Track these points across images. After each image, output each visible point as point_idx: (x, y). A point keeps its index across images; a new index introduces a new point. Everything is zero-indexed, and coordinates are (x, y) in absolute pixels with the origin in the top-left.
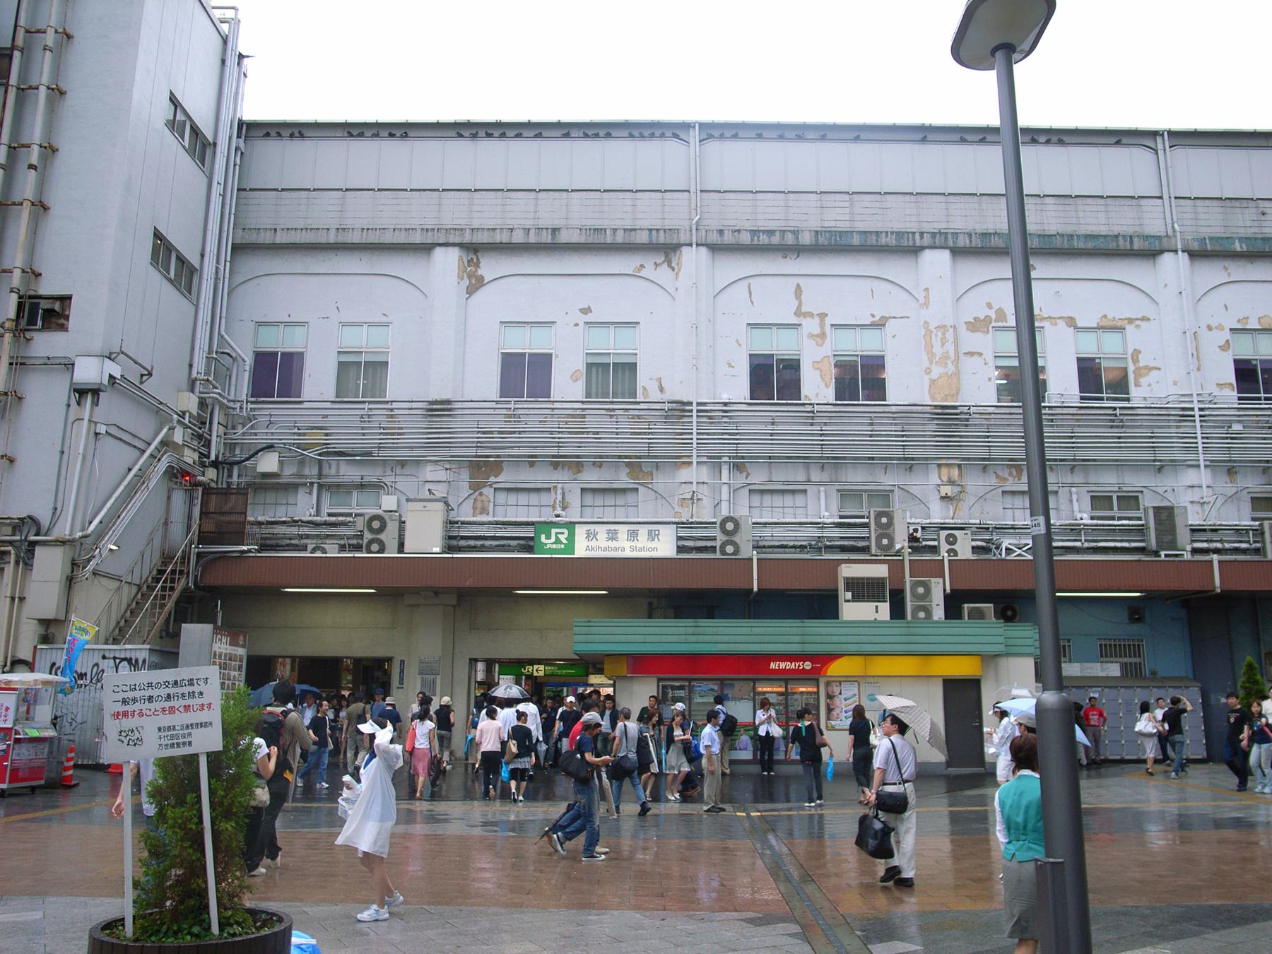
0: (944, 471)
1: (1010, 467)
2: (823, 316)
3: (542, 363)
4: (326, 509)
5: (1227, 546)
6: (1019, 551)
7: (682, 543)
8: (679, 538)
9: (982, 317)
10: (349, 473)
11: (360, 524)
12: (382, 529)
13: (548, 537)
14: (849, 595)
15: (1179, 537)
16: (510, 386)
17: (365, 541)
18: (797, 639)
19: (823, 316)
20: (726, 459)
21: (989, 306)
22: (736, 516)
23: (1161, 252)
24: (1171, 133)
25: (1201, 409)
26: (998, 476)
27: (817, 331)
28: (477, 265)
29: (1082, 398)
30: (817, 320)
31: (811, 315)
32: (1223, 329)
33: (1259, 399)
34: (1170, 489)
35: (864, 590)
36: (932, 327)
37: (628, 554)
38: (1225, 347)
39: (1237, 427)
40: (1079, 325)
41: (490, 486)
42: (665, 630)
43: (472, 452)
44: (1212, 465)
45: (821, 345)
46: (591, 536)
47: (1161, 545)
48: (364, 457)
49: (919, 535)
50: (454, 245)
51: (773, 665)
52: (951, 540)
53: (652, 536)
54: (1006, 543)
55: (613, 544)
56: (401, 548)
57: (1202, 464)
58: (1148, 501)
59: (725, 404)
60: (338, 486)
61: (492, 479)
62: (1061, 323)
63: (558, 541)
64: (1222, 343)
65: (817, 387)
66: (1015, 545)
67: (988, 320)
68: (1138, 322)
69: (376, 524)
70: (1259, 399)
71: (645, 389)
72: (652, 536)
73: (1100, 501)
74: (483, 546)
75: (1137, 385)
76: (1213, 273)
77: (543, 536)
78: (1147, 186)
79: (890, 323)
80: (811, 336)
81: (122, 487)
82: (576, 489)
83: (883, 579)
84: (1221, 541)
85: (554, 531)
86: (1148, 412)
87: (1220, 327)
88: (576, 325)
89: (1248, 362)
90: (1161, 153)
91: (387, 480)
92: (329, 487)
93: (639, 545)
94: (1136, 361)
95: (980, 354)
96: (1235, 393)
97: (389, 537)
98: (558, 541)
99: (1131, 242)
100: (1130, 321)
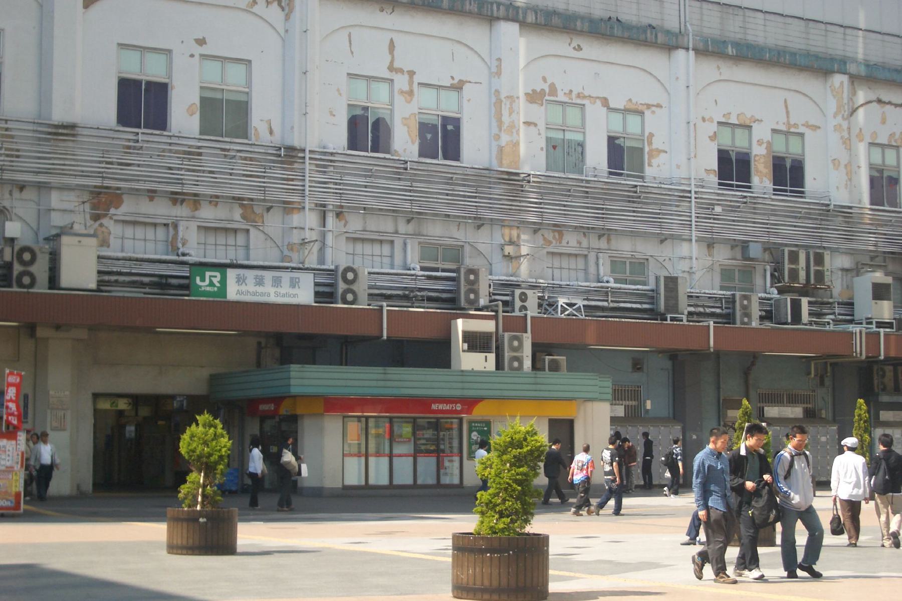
0: (507, 231)
1: (554, 231)
2: (412, 74)
5: (708, 310)
6: (570, 310)
7: (321, 289)
9: (538, 90)
13: (203, 280)
14: (466, 346)
15: (680, 302)
17: (340, 291)
18: (460, 385)
19: (412, 74)
20: (331, 207)
21: (544, 79)
22: (355, 267)
23: (677, 47)
25: (696, 192)
26: (545, 239)
27: (406, 88)
29: (610, 173)
30: (406, 77)
31: (400, 71)
32: (712, 122)
33: (786, 191)
34: (667, 259)
35: (476, 342)
36: (502, 97)
37: (273, 299)
38: (714, 137)
39: (718, 209)
40: (612, 106)
41: (111, 218)
42: (362, 376)
43: (97, 182)
44: (699, 240)
45: (409, 102)
46: (240, 280)
51: (434, 407)
53: (294, 283)
54: (562, 301)
55: (260, 289)
57: (694, 239)
58: (653, 271)
59: (332, 154)
62: (599, 102)
64: (711, 134)
65: (405, 143)
66: (567, 304)
68: (654, 109)
70: (786, 191)
71: (256, 130)
72: (294, 283)
73: (616, 265)
74: (116, 281)
76: (710, 69)
77: (198, 279)
79: (466, 87)
80: (402, 92)
82: (193, 225)
83: (491, 333)
84: (703, 306)
85: (208, 274)
86: (94, 132)
87: (711, 120)
88: (192, 56)
89: (727, 152)
93: (283, 291)
94: (650, 143)
95: (535, 125)
96: (771, 186)
98: (211, 284)
100: (649, 106)
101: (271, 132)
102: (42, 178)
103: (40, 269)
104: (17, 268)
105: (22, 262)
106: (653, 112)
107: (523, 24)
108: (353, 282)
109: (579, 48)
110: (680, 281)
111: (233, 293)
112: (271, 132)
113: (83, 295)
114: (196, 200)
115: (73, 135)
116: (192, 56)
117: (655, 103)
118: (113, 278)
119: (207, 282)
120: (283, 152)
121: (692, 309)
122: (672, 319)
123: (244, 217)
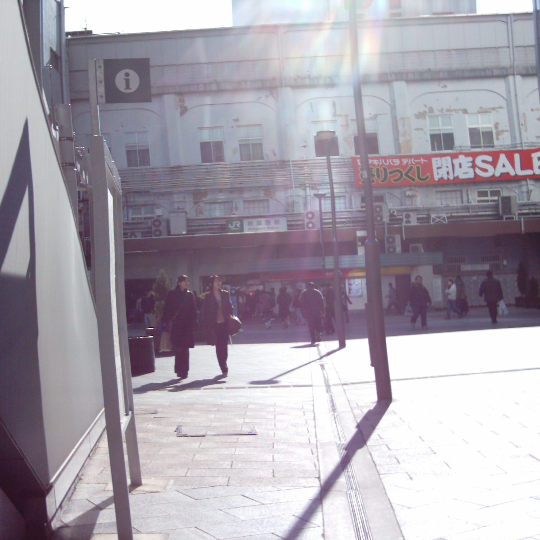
3: (219, 146)
4: (131, 216)
6: (438, 219)
7: (289, 223)
8: (288, 221)
9: (417, 113)
10: (140, 200)
11: (150, 222)
12: (160, 224)
13: (232, 225)
16: (206, 158)
20: (308, 185)
21: (425, 106)
24: (515, 15)
28: (183, 101)
43: (194, 188)
47: (504, 213)
48: (146, 193)
49: (395, 214)
50: (172, 93)
52: (408, 216)
54: (433, 216)
56: (169, 233)
60: (135, 206)
61: (203, 199)
62: (460, 112)
63: (236, 227)
67: (425, 113)
68: (498, 110)
69: (157, 223)
72: (276, 222)
75: (497, 139)
78: (502, 41)
81: (76, 447)
85: (234, 223)
90: (509, 24)
91: (157, 202)
92: (131, 206)
95: (422, 129)
97: (163, 228)
98: (236, 227)
99: (492, 72)
101: (275, 155)
102: (168, 190)
103: (163, 228)
104: (154, 228)
105: (155, 226)
106: (498, 112)
107: (408, 81)
108: (312, 218)
109: (445, 86)
110: (512, 199)
111: (247, 231)
112: (275, 155)
113: (147, 239)
114: (241, 190)
115: (181, 170)
116: (232, 127)
117: (498, 106)
118: (201, 228)
119: (234, 226)
120: (346, 161)
121: (520, 212)
122: (507, 218)
123: (266, 194)
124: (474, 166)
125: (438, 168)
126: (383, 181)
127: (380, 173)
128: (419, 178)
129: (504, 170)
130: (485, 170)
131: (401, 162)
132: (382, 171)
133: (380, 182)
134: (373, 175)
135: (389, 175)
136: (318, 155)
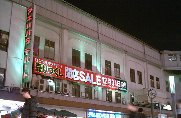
124: (79, 75)
125: (67, 72)
126: (45, 72)
127: (44, 68)
128: (59, 75)
129: (89, 80)
130: (82, 78)
131: (53, 65)
132: (45, 67)
133: (43, 72)
134: (41, 68)
135: (48, 70)
136: (111, 92)
